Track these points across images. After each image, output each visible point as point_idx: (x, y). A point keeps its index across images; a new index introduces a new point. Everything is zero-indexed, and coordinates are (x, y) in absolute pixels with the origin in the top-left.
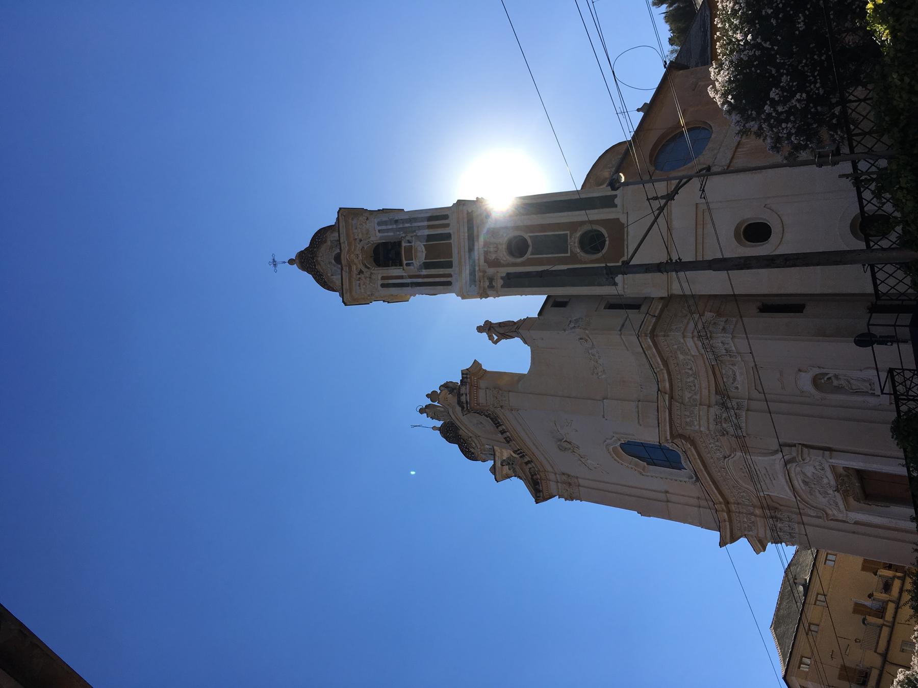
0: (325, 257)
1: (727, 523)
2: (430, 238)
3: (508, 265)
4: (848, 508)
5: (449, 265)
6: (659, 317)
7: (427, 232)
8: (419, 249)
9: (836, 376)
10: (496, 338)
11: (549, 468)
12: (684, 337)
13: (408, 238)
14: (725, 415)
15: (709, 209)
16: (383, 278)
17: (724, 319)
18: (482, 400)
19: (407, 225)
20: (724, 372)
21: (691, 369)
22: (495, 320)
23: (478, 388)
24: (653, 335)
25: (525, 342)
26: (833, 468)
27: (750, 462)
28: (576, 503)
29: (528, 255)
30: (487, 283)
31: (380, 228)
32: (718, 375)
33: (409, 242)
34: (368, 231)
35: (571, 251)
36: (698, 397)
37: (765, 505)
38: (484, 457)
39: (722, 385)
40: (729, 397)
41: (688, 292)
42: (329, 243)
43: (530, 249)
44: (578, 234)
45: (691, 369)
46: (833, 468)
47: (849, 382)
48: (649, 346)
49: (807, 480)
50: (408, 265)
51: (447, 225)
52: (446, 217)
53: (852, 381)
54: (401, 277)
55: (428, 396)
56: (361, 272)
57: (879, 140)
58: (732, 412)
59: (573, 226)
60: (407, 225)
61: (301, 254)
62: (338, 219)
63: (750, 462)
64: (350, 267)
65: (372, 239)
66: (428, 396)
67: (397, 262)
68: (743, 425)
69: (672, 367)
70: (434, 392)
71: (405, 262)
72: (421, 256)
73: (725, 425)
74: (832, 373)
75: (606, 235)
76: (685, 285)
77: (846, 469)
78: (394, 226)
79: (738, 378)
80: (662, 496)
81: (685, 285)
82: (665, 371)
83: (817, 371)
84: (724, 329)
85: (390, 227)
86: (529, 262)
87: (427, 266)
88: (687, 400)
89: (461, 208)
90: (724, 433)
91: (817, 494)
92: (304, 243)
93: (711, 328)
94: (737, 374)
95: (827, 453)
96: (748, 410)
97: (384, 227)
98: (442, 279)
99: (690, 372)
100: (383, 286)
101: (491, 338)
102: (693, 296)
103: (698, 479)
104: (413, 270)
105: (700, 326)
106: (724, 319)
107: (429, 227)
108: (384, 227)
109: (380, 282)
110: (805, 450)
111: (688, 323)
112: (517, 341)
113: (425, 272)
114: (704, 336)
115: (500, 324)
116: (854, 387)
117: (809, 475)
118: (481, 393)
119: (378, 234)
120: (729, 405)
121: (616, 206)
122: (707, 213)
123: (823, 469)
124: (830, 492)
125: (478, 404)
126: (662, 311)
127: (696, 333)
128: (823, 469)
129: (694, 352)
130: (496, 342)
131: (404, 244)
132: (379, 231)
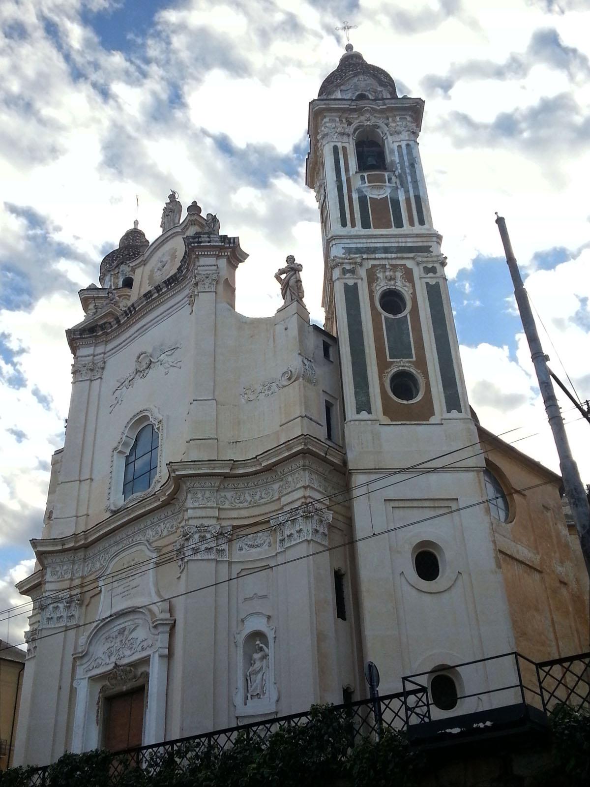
0: (363, 82)
1: (59, 548)
2: (396, 203)
3: (371, 293)
4: (92, 679)
5: (366, 225)
6: (324, 460)
7: (402, 197)
9: (265, 656)
10: (283, 276)
11: (110, 346)
13: (393, 178)
14: (208, 536)
15: (452, 512)
16: (344, 149)
17: (326, 532)
18: (203, 261)
19: (409, 178)
20: (259, 534)
21: (261, 498)
22: (303, 275)
24: (304, 453)
25: (279, 311)
26: (146, 661)
27: (144, 568)
28: (70, 378)
29: (384, 314)
30: (348, 267)
31: (404, 146)
32: (255, 529)
33: (390, 180)
34: (399, 133)
35: (392, 363)
36: (227, 506)
37: (85, 589)
38: (102, 271)
39: (243, 533)
40: (230, 541)
41: (356, 493)
42: (379, 89)
43: (391, 316)
44: (413, 370)
45: (261, 498)
46: (146, 661)
47: (259, 672)
48: (214, 468)
49: (126, 633)
50: (363, 178)
51: (412, 223)
52: (422, 222)
53: (260, 675)
54: (347, 170)
55: (195, 203)
56: (350, 124)
57: (580, 678)
58: (213, 544)
59: (421, 363)
60: (409, 178)
61: (358, 56)
62: (411, 99)
63: (144, 568)
65: (390, 139)
66: (195, 203)
67: (363, 166)
68: (199, 557)
69: (263, 476)
70: (199, 210)
71: (365, 175)
72: (374, 194)
73: (197, 536)
74: (270, 651)
75: (410, 402)
76: (364, 490)
77: (146, 675)
79: (253, 550)
80: (86, 475)
81: (364, 490)
82: (258, 468)
83: (270, 635)
84: (317, 531)
85: (406, 158)
86: (376, 316)
87: (363, 200)
88: (223, 494)
89: (435, 239)
90: (187, 537)
91: (108, 645)
92: (370, 59)
93: (316, 517)
94: (258, 549)
95: (166, 651)
96: (217, 561)
97: (405, 152)
98: (348, 216)
99: (257, 497)
100: (335, 149)
101: (282, 272)
102: (351, 499)
103: (115, 513)
104: (357, 183)
105: (318, 506)
106: (326, 532)
107: (408, 200)
108: (405, 152)
109: (339, 145)
110: (167, 629)
111: (319, 491)
112: (280, 302)
113: (355, 196)
114: (308, 511)
115: (299, 281)
117: (134, 635)
118: (212, 261)
119: (396, 144)
120: (221, 541)
121: (449, 411)
122: (447, 510)
123: (143, 649)
124: (113, 659)
125: (198, 257)
126: (332, 464)
127: (309, 500)
128: (143, 649)
129: (285, 500)
130: (277, 277)
131: (386, 174)
132: (399, 146)
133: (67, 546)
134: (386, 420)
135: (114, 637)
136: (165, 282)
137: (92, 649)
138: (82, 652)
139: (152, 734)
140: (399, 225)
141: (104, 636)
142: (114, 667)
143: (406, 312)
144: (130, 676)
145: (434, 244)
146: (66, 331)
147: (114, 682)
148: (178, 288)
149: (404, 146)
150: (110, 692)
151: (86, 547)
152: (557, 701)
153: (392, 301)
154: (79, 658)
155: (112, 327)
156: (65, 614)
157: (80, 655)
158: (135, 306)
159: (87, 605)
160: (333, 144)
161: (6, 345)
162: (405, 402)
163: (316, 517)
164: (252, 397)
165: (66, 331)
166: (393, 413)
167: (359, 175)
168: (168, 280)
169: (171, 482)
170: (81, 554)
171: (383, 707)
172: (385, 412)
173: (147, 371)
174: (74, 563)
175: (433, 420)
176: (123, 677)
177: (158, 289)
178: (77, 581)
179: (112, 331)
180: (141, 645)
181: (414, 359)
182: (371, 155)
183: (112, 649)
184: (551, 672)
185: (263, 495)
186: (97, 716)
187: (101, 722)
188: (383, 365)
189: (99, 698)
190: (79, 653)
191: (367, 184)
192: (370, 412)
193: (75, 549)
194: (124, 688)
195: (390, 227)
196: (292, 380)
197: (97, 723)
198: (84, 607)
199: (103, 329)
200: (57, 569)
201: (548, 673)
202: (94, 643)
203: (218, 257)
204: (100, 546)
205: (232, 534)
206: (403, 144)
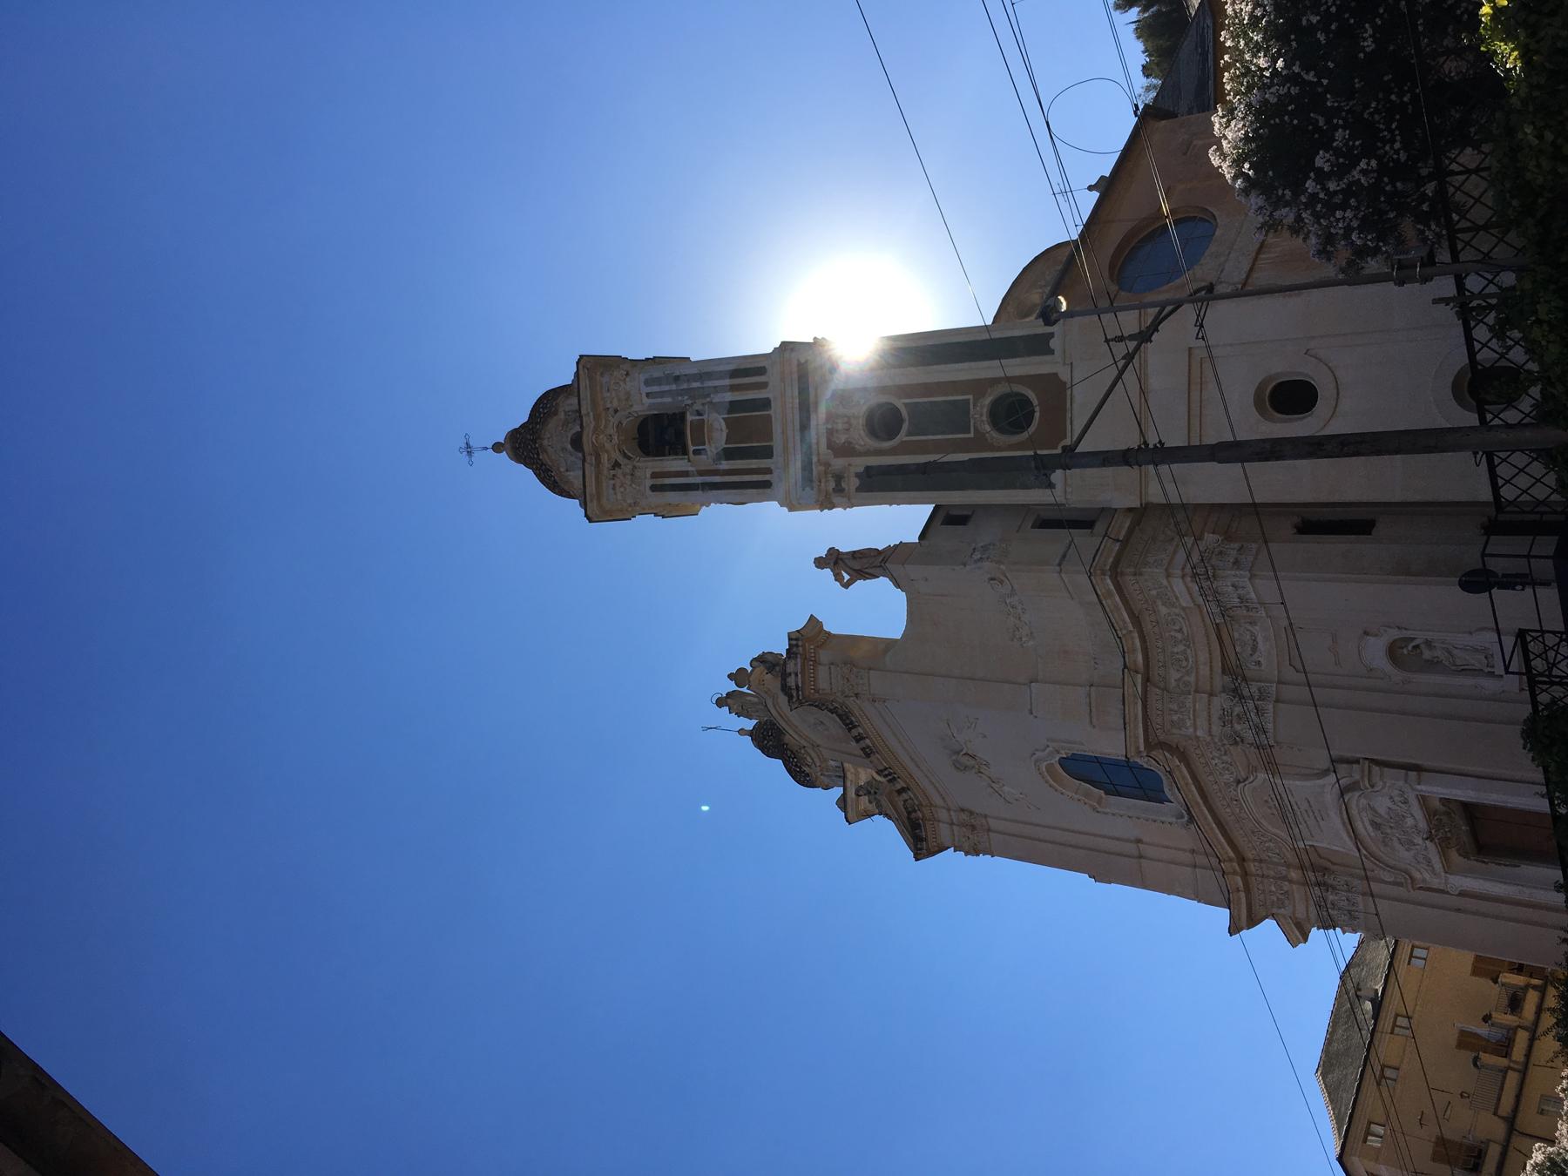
0: (555, 440)
1: (1242, 895)
2: (734, 406)
3: (868, 453)
4: (1448, 869)
5: (767, 453)
6: (1125, 543)
7: (729, 397)
9: (1429, 644)
10: (847, 577)
11: (938, 801)
12: (1168, 576)
13: (696, 407)
14: (1238, 710)
15: (1211, 357)
16: (654, 475)
17: (1236, 546)
18: (823, 684)
19: (695, 385)
20: (1236, 635)
21: (1180, 630)
22: (845, 548)
24: (1115, 573)
25: (898, 585)
26: (1423, 800)
27: (1281, 789)
28: (984, 859)
29: (902, 436)
30: (832, 484)
31: (649, 390)
32: (1227, 641)
33: (699, 413)
34: (628, 394)
35: (976, 430)
37: (1307, 864)
38: (826, 780)
39: (1233, 657)
40: (1245, 679)
41: (1175, 500)
42: (562, 415)
43: (905, 426)
44: (988, 400)
45: (1180, 630)
46: (1423, 800)
47: (1449, 653)
48: (1109, 591)
49: (1378, 820)
50: (696, 452)
51: (764, 385)
52: (761, 371)
53: (1455, 652)
54: (686, 474)
55: (730, 676)
57: (1501, 240)
58: (1251, 705)
59: (978, 387)
60: (695, 385)
61: (514, 435)
63: (1281, 789)
64: (598, 457)
65: (636, 408)
66: (730, 676)
67: (679, 448)
68: (1270, 726)
69: (1148, 627)
71: (691, 448)
72: (719, 437)
73: (1238, 727)
74: (1420, 637)
75: (1035, 402)
76: (1170, 487)
77: (1445, 801)
78: (674, 387)
79: (1261, 645)
80: (1131, 848)
81: (1170, 487)
82: (1136, 635)
83: (1395, 634)
84: (1236, 562)
85: (667, 388)
86: (904, 448)
87: (729, 454)
88: (1174, 684)
89: (787, 355)
90: (1237, 740)
91: (1396, 844)
92: (520, 416)
93: (1214, 561)
94: (1260, 639)
95: (1413, 774)
96: (1277, 701)
97: (655, 389)
98: (755, 478)
100: (654, 488)
101: (838, 578)
102: (1184, 506)
104: (705, 461)
105: (1196, 558)
106: (1236, 546)
107: (733, 388)
108: (655, 389)
109: (649, 482)
111: (1175, 552)
112: (883, 583)
113: (725, 465)
114: (1202, 574)
115: (854, 555)
117: (1382, 811)
118: (822, 672)
119: (645, 400)
120: (1246, 692)
121: (1052, 352)
122: (1207, 365)
123: (1406, 802)
124: (1418, 840)
125: (817, 691)
126: (1130, 531)
127: (1188, 570)
128: (1406, 802)
129: (1185, 601)
130: (846, 585)
131: (689, 418)
132: (648, 395)
139: (1534, 801)
161: (796, 363)
163: (1214, 561)
169: (1153, 753)
184: (1473, 243)
203: (816, 663)
205: (1236, 679)
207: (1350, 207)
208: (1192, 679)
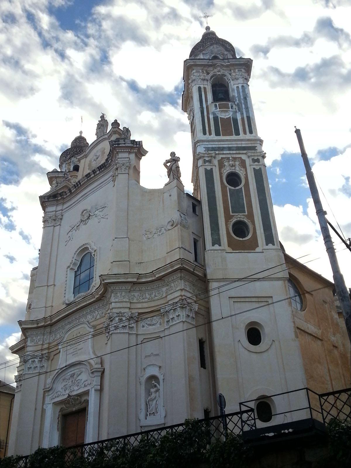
0: (216, 49)
1: (35, 326)
2: (235, 121)
3: (221, 174)
4: (55, 404)
5: (217, 134)
6: (193, 273)
7: (239, 117)
8: (227, 114)
9: (158, 390)
10: (168, 164)
11: (66, 206)
12: (181, 290)
13: (234, 106)
14: (124, 319)
15: (269, 304)
16: (205, 88)
17: (194, 316)
18: (121, 155)
19: (243, 106)
20: (154, 318)
21: (155, 296)
22: (180, 164)
23: (130, 153)
24: (181, 269)
25: (166, 185)
26: (87, 393)
27: (86, 338)
28: (42, 225)
29: (228, 187)
31: (240, 87)
32: (152, 315)
33: (232, 107)
34: (237, 79)
35: (233, 216)
37: (51, 350)
38: (61, 161)
39: (145, 317)
40: (137, 321)
41: (212, 293)
42: (226, 53)
43: (233, 188)
44: (246, 220)
45: (155, 296)
46: (87, 393)
47: (154, 399)
49: (75, 376)
50: (216, 106)
51: (245, 133)
52: (251, 132)
53: (155, 402)
54: (206, 101)
55: (116, 121)
57: (345, 403)
58: (127, 324)
59: (251, 216)
60: (243, 106)
61: (213, 34)
63: (86, 338)
64: (211, 66)
65: (232, 82)
66: (116, 121)
67: (216, 99)
68: (118, 331)
69: (157, 283)
71: (217, 104)
72: (222, 116)
73: (117, 319)
74: (161, 387)
75: (244, 239)
76: (216, 291)
77: (87, 402)
78: (242, 97)
79: (151, 327)
80: (51, 282)
81: (216, 291)
82: (153, 278)
83: (161, 378)
84: (188, 316)
85: (241, 94)
86: (223, 188)
87: (216, 119)
88: (132, 294)
89: (258, 142)
90: (111, 319)
91: (64, 384)
92: (220, 35)
93: (188, 308)
94: (154, 327)
95: (99, 387)
96: (129, 334)
97: (241, 90)
98: (207, 128)
100: (200, 88)
101: (168, 162)
102: (209, 297)
104: (212, 109)
105: (189, 301)
106: (194, 316)
107: (243, 119)
108: (241, 90)
109: (202, 86)
111: (190, 292)
112: (167, 180)
113: (211, 117)
114: (183, 304)
115: (178, 167)
116: (150, 402)
117: (79, 378)
118: (126, 155)
119: (236, 86)
120: (131, 322)
121: (267, 245)
122: (266, 304)
123: (85, 386)
124: (67, 392)
125: (118, 153)
126: (197, 276)
127: (184, 297)
128: (85, 386)
129: (170, 297)
130: (165, 165)
131: (230, 104)
132: (238, 87)
133: (40, 325)
134: (230, 250)
135: (68, 379)
136: (98, 168)
137: (54, 386)
138: (49, 388)
139: (90, 437)
140: (238, 134)
141: (62, 378)
142: (68, 397)
143: (242, 185)
144: (78, 402)
145: (258, 145)
146: (39, 197)
147: (68, 405)
148: (106, 171)
149: (240, 87)
150: (65, 412)
151: (51, 325)
152: (331, 417)
153: (233, 179)
154: (47, 391)
155: (66, 194)
156: (38, 365)
157: (48, 390)
158: (80, 182)
159: (52, 360)
160: (198, 86)
162: (241, 239)
164: (150, 236)
165: (39, 197)
166: (234, 246)
167: (213, 104)
168: (100, 166)
170: (48, 330)
171: (228, 420)
172: (229, 245)
173: (87, 221)
174: (44, 335)
175: (257, 250)
176: (73, 403)
177: (94, 172)
178: (46, 345)
179: (67, 197)
180: (84, 384)
181: (246, 213)
182: (221, 92)
183: (67, 386)
185: (157, 295)
186: (58, 426)
187: (60, 429)
188: (228, 217)
189: (59, 415)
190: (47, 388)
191: (218, 110)
192: (220, 245)
193: (44, 327)
194: (74, 409)
195: (232, 135)
196: (174, 226)
197: (58, 430)
198: (50, 361)
199: (61, 196)
200: (34, 339)
201: (326, 400)
202: (56, 382)
204: (60, 325)
206: (240, 86)
207: (186, 434)
208: (135, 301)
